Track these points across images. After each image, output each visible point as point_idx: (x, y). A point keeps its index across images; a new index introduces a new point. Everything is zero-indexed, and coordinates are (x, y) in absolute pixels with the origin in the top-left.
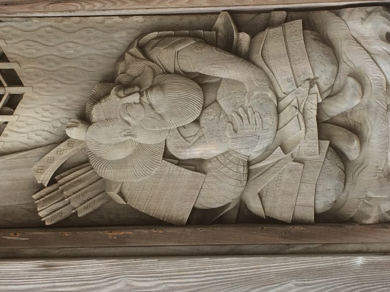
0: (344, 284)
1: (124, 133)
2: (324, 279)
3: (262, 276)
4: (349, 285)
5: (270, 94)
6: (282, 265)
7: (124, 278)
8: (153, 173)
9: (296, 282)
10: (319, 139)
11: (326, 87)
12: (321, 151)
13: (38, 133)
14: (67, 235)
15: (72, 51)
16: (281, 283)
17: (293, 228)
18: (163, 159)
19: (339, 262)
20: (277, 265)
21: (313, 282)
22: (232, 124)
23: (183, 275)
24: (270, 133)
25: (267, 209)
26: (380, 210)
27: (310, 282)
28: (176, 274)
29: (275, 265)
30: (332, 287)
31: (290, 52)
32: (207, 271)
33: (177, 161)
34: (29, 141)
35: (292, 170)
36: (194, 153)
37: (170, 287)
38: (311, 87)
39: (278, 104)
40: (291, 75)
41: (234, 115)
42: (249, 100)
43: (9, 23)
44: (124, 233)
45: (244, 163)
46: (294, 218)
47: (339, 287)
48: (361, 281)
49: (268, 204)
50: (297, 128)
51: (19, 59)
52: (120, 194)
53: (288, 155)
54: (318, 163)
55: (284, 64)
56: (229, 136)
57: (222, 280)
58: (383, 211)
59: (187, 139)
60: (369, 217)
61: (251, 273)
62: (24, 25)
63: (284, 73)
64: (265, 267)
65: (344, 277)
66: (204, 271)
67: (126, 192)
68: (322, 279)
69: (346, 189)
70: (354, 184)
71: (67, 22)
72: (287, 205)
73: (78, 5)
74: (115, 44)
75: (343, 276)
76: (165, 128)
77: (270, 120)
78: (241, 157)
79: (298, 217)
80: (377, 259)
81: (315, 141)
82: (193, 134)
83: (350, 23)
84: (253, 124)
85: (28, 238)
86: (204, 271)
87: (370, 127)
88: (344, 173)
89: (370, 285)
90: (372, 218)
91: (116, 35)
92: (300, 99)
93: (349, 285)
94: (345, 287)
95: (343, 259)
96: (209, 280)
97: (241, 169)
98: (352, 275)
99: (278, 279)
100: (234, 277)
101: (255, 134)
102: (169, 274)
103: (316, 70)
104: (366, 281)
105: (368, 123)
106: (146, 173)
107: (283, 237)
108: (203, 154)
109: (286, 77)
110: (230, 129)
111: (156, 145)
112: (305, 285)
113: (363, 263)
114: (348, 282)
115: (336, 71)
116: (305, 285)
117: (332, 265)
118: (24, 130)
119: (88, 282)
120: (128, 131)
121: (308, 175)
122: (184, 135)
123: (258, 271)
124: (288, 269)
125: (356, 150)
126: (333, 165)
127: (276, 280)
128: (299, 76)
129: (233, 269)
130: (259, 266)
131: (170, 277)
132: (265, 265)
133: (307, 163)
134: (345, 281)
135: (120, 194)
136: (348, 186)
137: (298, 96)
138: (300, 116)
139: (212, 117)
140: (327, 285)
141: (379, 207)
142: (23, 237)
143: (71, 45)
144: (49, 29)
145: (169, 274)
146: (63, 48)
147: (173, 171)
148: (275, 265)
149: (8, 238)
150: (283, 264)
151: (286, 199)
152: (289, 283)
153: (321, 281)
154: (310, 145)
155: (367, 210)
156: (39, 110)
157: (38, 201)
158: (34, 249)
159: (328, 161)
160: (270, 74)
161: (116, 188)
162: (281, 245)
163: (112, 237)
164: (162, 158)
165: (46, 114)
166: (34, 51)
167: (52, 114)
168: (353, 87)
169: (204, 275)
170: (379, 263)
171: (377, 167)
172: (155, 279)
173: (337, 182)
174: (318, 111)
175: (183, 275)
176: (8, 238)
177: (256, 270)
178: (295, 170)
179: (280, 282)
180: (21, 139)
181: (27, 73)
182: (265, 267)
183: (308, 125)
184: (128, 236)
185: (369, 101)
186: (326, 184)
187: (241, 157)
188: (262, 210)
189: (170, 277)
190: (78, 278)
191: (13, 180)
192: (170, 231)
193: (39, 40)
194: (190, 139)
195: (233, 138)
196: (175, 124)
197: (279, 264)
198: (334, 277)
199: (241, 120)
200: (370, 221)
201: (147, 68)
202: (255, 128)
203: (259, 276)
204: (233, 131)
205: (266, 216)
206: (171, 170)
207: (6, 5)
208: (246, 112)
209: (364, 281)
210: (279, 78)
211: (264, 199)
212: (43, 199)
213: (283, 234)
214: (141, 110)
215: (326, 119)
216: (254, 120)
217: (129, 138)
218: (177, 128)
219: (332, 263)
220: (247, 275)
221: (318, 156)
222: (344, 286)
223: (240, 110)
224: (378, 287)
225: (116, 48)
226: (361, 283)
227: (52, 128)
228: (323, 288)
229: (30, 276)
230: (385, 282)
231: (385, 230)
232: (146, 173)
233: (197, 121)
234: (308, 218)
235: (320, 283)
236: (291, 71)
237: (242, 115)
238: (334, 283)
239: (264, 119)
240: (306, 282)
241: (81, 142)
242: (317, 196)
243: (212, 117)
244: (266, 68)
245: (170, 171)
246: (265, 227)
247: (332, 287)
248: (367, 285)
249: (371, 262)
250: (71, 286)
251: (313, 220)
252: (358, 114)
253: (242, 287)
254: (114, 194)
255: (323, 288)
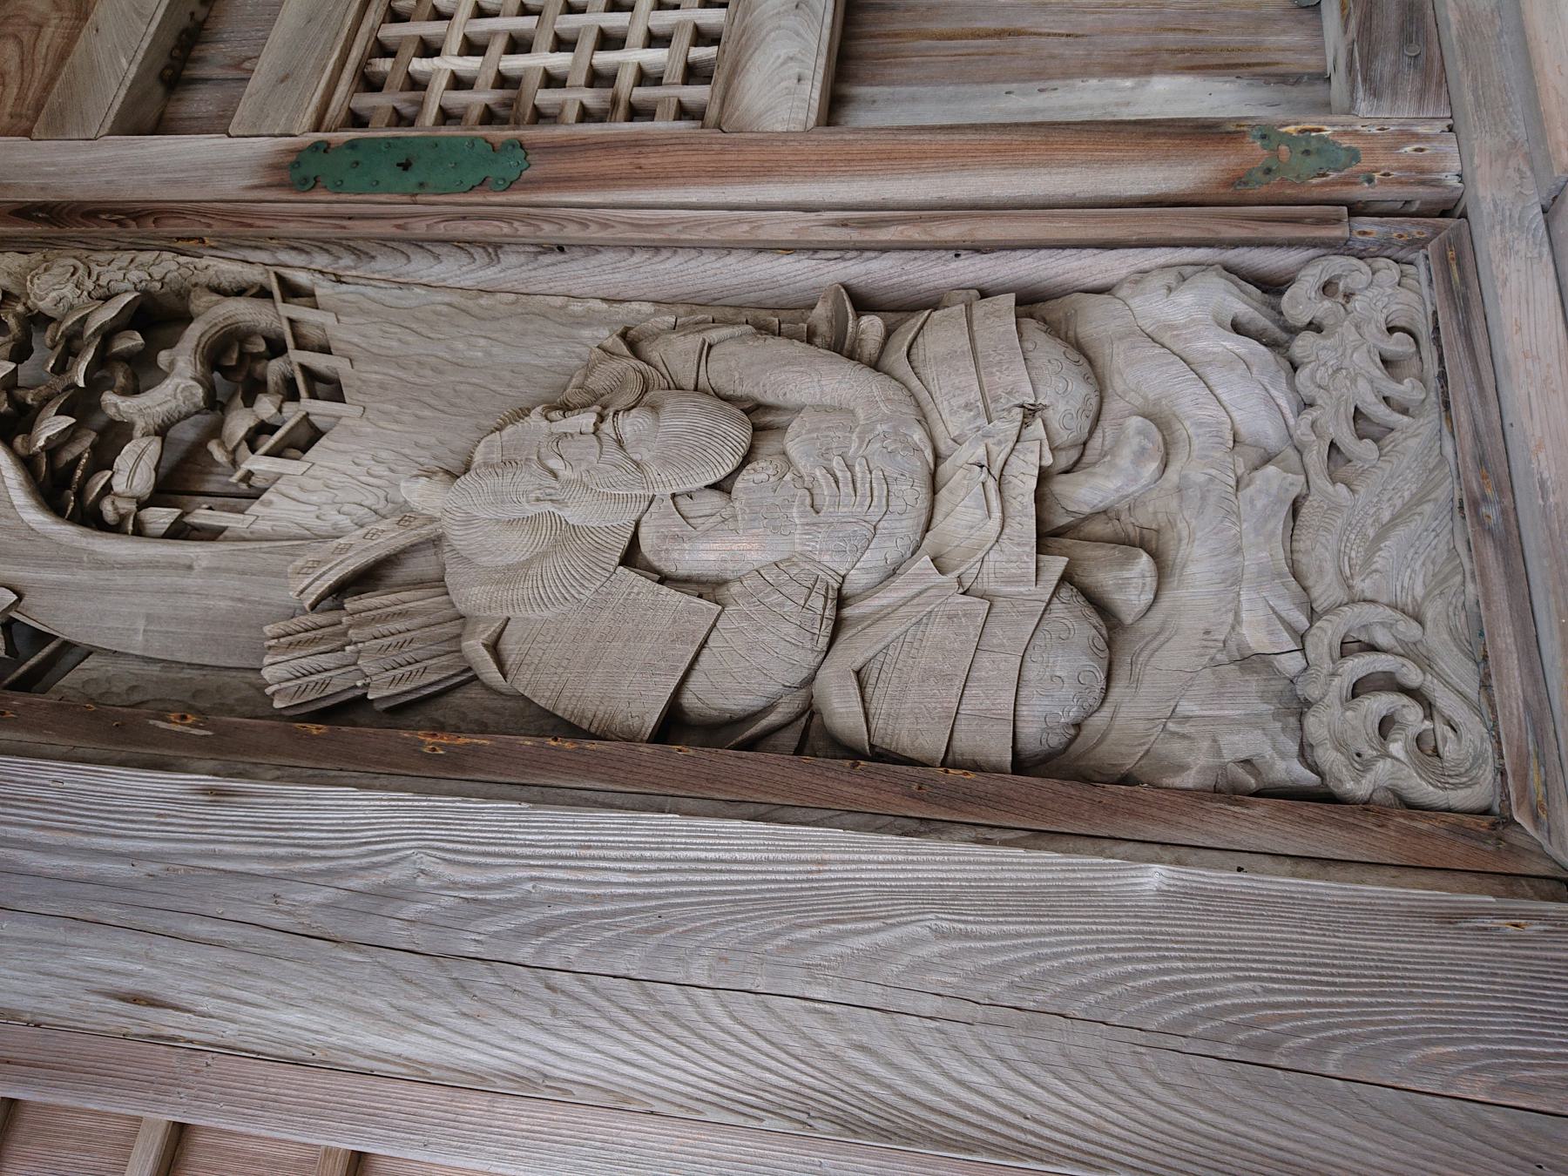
0: (1099, 950)
1: (538, 493)
2: (1032, 923)
3: (830, 888)
4: (1116, 955)
5: (918, 435)
6: (898, 862)
7: (416, 851)
8: (587, 593)
9: (939, 923)
10: (1038, 552)
11: (1064, 437)
12: (1040, 578)
13: (346, 508)
14: (315, 732)
15: (480, 354)
16: (889, 921)
17: (947, 772)
18: (621, 564)
19: (1084, 875)
20: (881, 858)
21: (994, 929)
22: (812, 494)
23: (593, 858)
24: (904, 523)
25: (878, 723)
26: (1218, 752)
27: (984, 929)
28: (573, 852)
29: (875, 857)
30: (1056, 956)
31: (979, 349)
32: (667, 854)
33: (657, 577)
34: (319, 522)
35: (956, 616)
36: (704, 556)
37: (548, 891)
38: (1025, 424)
39: (936, 465)
40: (975, 394)
41: (818, 473)
42: (861, 440)
43: (362, 289)
44: (468, 740)
45: (827, 589)
46: (950, 757)
47: (1083, 958)
48: (1160, 949)
49: (880, 706)
50: (980, 514)
51: (354, 353)
52: (494, 648)
53: (949, 576)
54: (1032, 604)
55: (961, 371)
56: (797, 521)
57: (705, 888)
58: (1228, 756)
59: (691, 521)
60: (1182, 768)
61: (798, 877)
62: (391, 295)
63: (958, 392)
64: (843, 862)
65: (1100, 928)
66: (656, 854)
67: (509, 646)
68: (1026, 923)
69: (1111, 699)
70: (1135, 681)
71: (485, 301)
72: (935, 708)
73: (503, 225)
74: (579, 349)
75: (1095, 923)
76: (642, 492)
77: (911, 494)
78: (820, 573)
79: (962, 755)
80: (1215, 881)
81: (1027, 549)
82: (708, 512)
83: (1135, 303)
84: (863, 496)
85: (209, 730)
86: (656, 854)
87: (1185, 533)
88: (1109, 647)
89: (1191, 965)
90: (1193, 772)
91: (586, 333)
92: (994, 449)
93: (1116, 955)
94: (1101, 960)
95: (1097, 864)
96: (667, 884)
97: (817, 602)
98: (1127, 924)
99: (880, 906)
100: (742, 883)
101: (867, 518)
102: (552, 851)
103: (1041, 388)
104: (1174, 949)
105: (1181, 525)
106: (569, 592)
107: (912, 796)
108: (725, 561)
109: (962, 401)
110: (803, 503)
111: (609, 530)
112: (967, 936)
113: (1166, 888)
114: (1112, 946)
115: (1094, 401)
116: (967, 936)
117: (1060, 879)
118: (314, 498)
119: (312, 852)
120: (548, 491)
121: (999, 633)
122: (685, 514)
123: (819, 871)
124: (915, 875)
125: (1143, 577)
126: (1076, 617)
127: (874, 906)
128: (996, 400)
129: (745, 856)
130: (826, 856)
131: (553, 862)
132: (846, 857)
133: (1000, 604)
134: (1102, 941)
135: (494, 648)
136: (1117, 692)
137: (990, 441)
138: (992, 485)
139: (764, 476)
140: (1042, 944)
141: (1215, 741)
142: (200, 728)
143: (482, 342)
144: (445, 309)
145: (552, 851)
146: (460, 345)
147: (638, 594)
148: (875, 857)
149: (162, 725)
150: (901, 858)
151: (931, 693)
152: (912, 922)
153: (1021, 928)
154: (1014, 558)
155: (1177, 748)
156: (365, 459)
157: (273, 642)
158: (213, 762)
159: (1061, 606)
160: (923, 395)
161: (483, 632)
162: (905, 821)
163: (434, 750)
164: (618, 560)
165: (380, 470)
166: (395, 344)
167: (392, 471)
168: (1140, 432)
169: (653, 866)
170: (1222, 894)
171: (1207, 632)
172: (507, 861)
173: (1084, 661)
174: (1039, 497)
175: (593, 858)
176: (162, 725)
177: (814, 868)
178: (965, 615)
179: (885, 917)
180: (301, 518)
181: (363, 381)
182: (843, 862)
183: (1010, 511)
184: (477, 748)
185: (1183, 477)
186: (1051, 660)
187: (820, 573)
188: (863, 719)
189: (553, 862)
190: (288, 838)
191: (240, 600)
192: (594, 747)
193: (414, 326)
194: (700, 521)
195: (807, 524)
196: (667, 484)
197: (889, 857)
198: (1066, 923)
199: (834, 485)
200: (1188, 780)
201: (631, 374)
202: (867, 503)
203: (823, 888)
204: (809, 508)
205: (872, 746)
206: (636, 590)
207: (350, 218)
208: (850, 467)
209: (1167, 949)
210: (944, 407)
211: (869, 690)
212: (290, 638)
213: (915, 787)
214: (592, 447)
215: (1063, 520)
216: (868, 485)
217: (549, 507)
218: (674, 496)
219: (1061, 875)
220: (787, 881)
221: (1033, 588)
222: (1097, 956)
223: (837, 464)
224: (1217, 975)
225: (579, 357)
226: (1159, 957)
227: (383, 502)
228: (1027, 953)
229: (159, 815)
230: (1244, 960)
231: (1236, 809)
232: (569, 592)
233: (721, 487)
234: (993, 759)
235: (1019, 935)
236: (976, 387)
237: (839, 474)
238: (1063, 944)
239: (894, 488)
240: (969, 927)
241: (432, 520)
242: (1022, 693)
243: (764, 476)
244: (915, 383)
245: (629, 594)
246: (862, 763)
247: (1056, 956)
248: (1180, 964)
249: (1192, 888)
250: (260, 858)
251: (1009, 765)
252: (1150, 509)
253: (761, 917)
254: (475, 648)
255: (1027, 953)
